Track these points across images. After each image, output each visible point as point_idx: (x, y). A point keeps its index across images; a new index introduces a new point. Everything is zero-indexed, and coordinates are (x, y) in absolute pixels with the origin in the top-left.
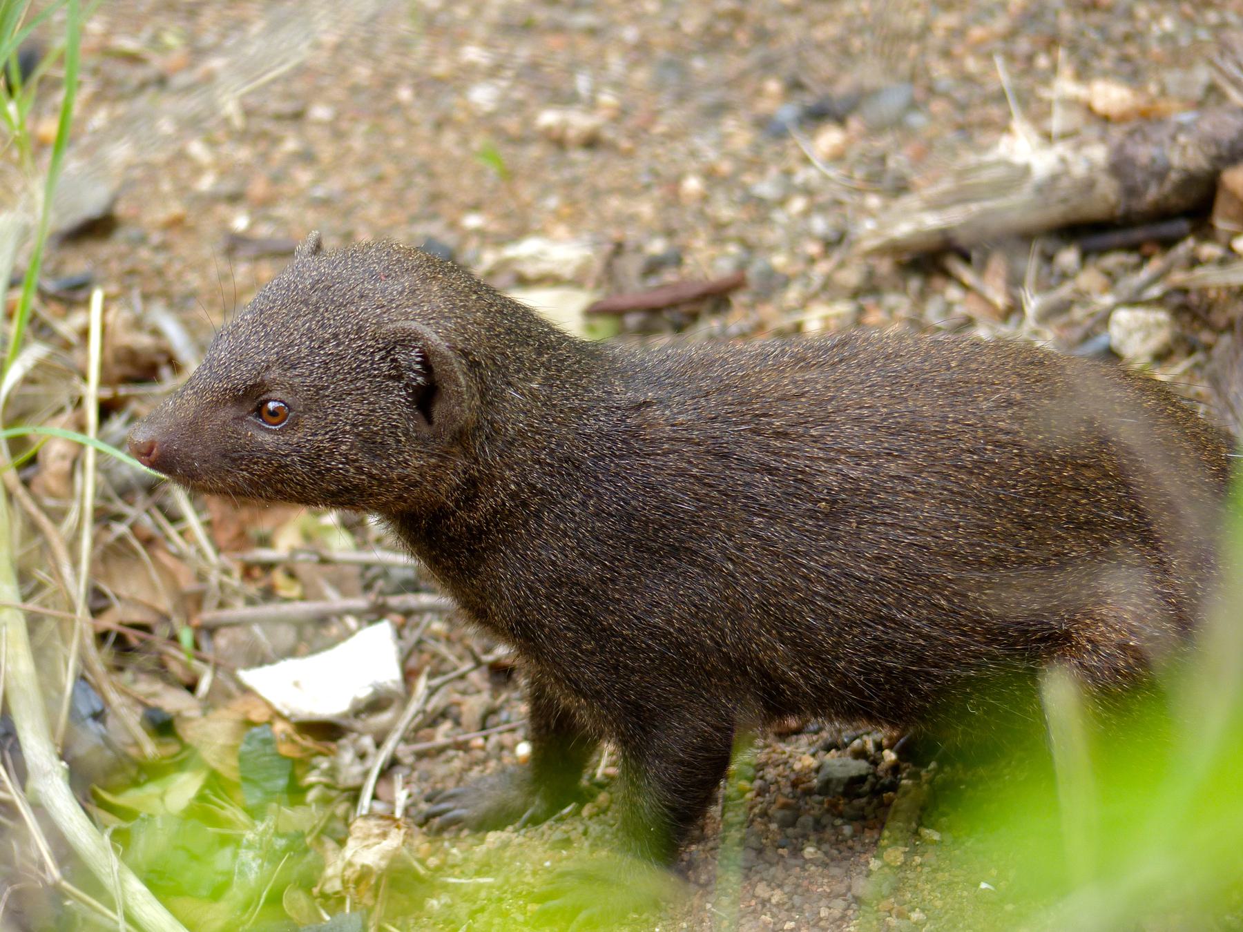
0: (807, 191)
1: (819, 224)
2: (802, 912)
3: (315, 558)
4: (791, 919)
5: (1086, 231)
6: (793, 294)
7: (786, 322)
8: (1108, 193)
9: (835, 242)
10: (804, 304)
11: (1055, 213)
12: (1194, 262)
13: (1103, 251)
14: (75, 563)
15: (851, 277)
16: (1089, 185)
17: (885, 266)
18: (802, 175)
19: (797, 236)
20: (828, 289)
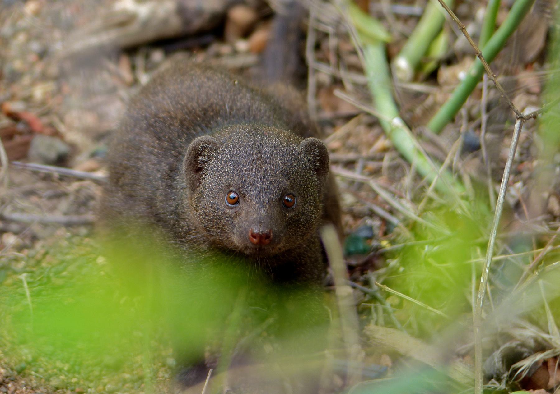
0: (26, 30)
1: (35, 46)
2: (79, 373)
3: (450, 126)
4: (74, 377)
5: (167, 43)
6: (26, 80)
7: (25, 93)
8: (175, 25)
9: (43, 55)
10: (33, 83)
11: (151, 34)
12: (218, 55)
13: (175, 51)
14: (523, 328)
15: (53, 70)
16: (165, 21)
17: (67, 66)
18: (22, 23)
19: (24, 52)
20: (44, 77)
